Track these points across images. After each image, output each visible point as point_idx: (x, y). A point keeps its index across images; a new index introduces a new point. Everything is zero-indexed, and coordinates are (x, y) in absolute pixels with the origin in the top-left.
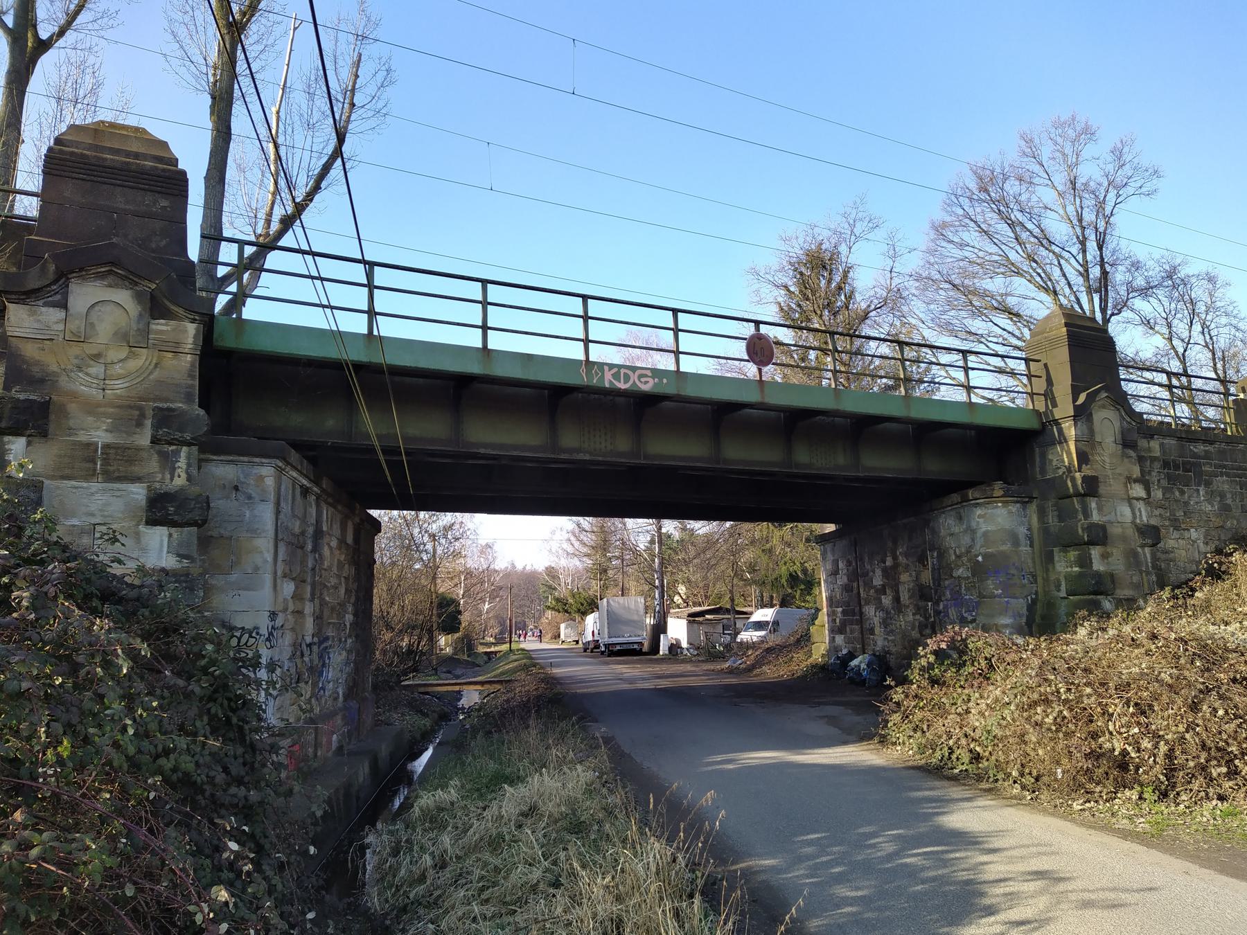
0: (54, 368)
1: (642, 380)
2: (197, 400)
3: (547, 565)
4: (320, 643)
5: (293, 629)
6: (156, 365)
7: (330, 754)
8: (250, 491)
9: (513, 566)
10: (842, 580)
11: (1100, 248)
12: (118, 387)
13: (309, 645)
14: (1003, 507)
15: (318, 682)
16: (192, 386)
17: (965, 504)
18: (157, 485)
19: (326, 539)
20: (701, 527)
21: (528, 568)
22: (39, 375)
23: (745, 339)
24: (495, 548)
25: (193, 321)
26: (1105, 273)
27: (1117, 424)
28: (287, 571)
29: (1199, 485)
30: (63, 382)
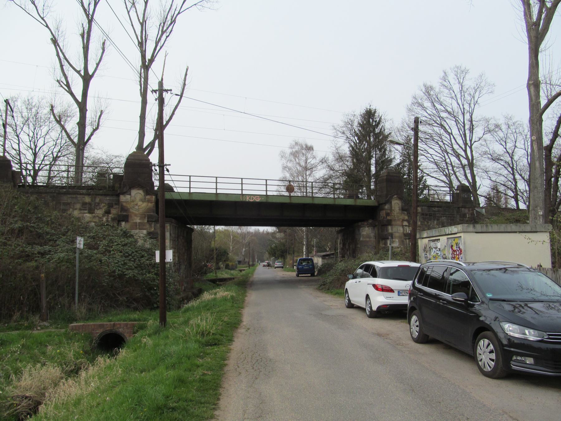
0: (129, 207)
12: (141, 211)
13: (177, 264)
27: (400, 204)
29: (435, 220)
30: (131, 210)
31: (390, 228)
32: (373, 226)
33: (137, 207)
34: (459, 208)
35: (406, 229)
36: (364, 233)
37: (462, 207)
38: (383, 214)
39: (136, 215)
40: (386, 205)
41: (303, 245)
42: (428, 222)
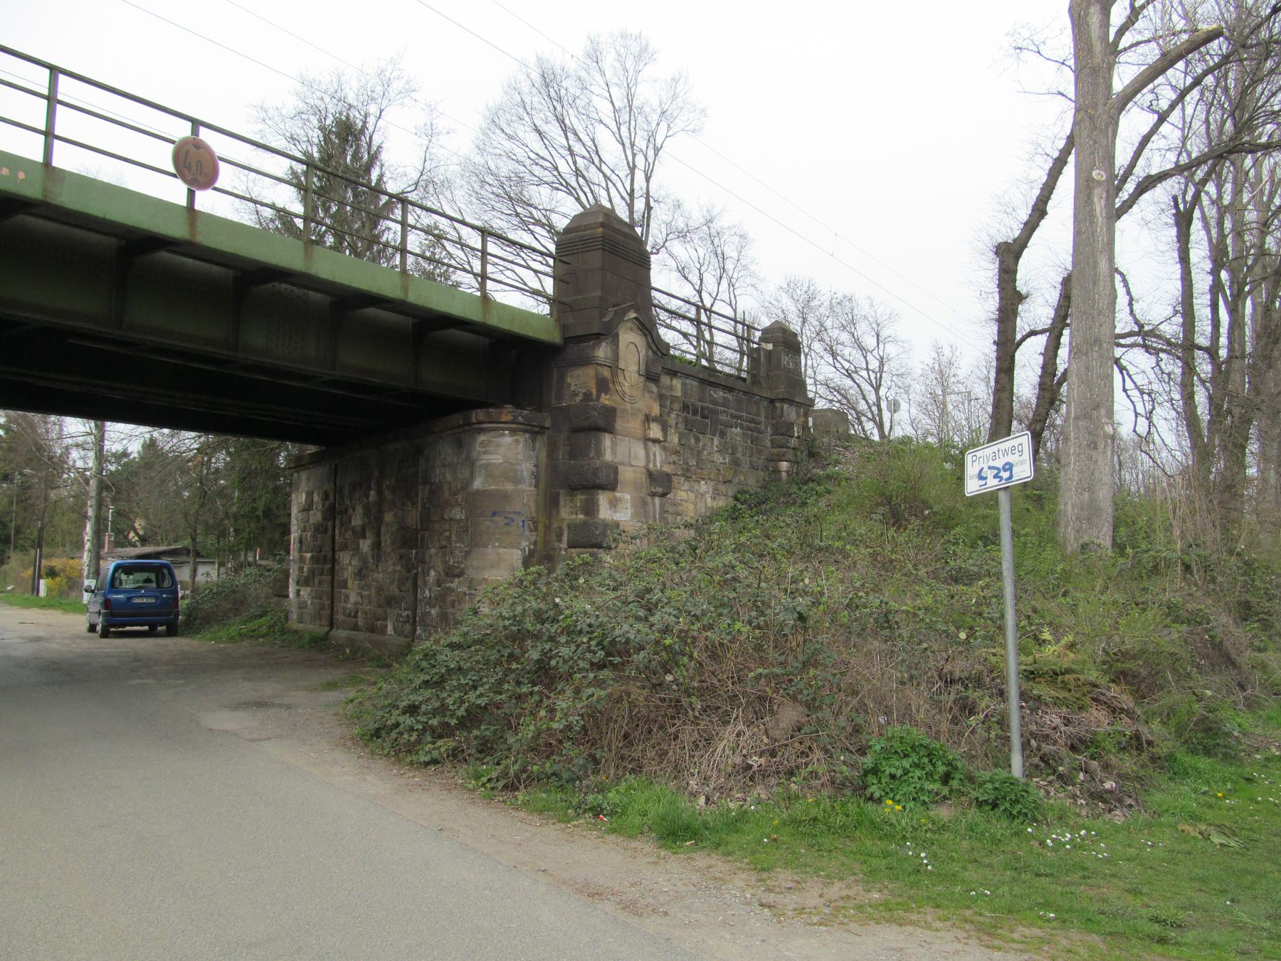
10: (316, 516)
11: (648, 179)
14: (511, 435)
17: (467, 428)
20: (189, 440)
23: (173, 142)
26: (649, 208)
31: (607, 440)
32: (534, 431)
34: (772, 401)
35: (655, 452)
36: (496, 458)
37: (783, 400)
38: (579, 380)
40: (598, 345)
41: (85, 517)
42: (697, 440)
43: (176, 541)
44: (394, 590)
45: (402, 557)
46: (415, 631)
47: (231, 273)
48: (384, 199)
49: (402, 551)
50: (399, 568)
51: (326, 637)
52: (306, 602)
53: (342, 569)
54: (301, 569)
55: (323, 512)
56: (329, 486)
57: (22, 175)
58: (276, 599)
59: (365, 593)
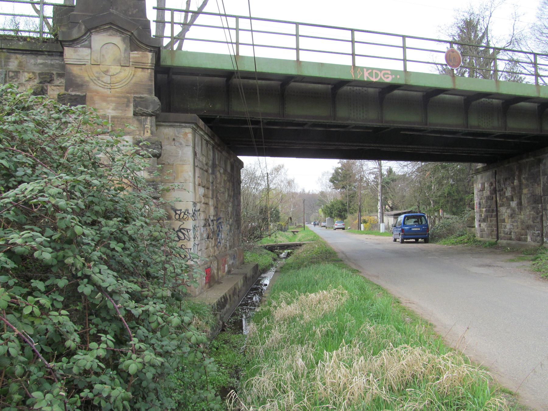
0: (87, 79)
1: (386, 76)
2: (154, 93)
3: (320, 190)
4: (218, 220)
5: (204, 212)
6: (134, 75)
7: (225, 274)
8: (181, 141)
9: (304, 190)
10: (487, 193)
13: (212, 221)
15: (217, 239)
16: (152, 85)
18: (137, 137)
19: (218, 168)
21: (311, 192)
22: (80, 83)
24: (295, 181)
25: (150, 51)
28: (200, 182)
30: (92, 86)
33: (107, 79)
39: (104, 98)
43: (407, 208)
44: (530, 222)
45: (534, 208)
46: (543, 240)
47: (463, 98)
48: (491, 51)
49: (534, 205)
50: (532, 213)
51: (496, 243)
52: (484, 229)
53: (502, 214)
54: (481, 216)
55: (490, 191)
56: (493, 180)
57: (398, 77)
58: (468, 228)
59: (515, 224)
